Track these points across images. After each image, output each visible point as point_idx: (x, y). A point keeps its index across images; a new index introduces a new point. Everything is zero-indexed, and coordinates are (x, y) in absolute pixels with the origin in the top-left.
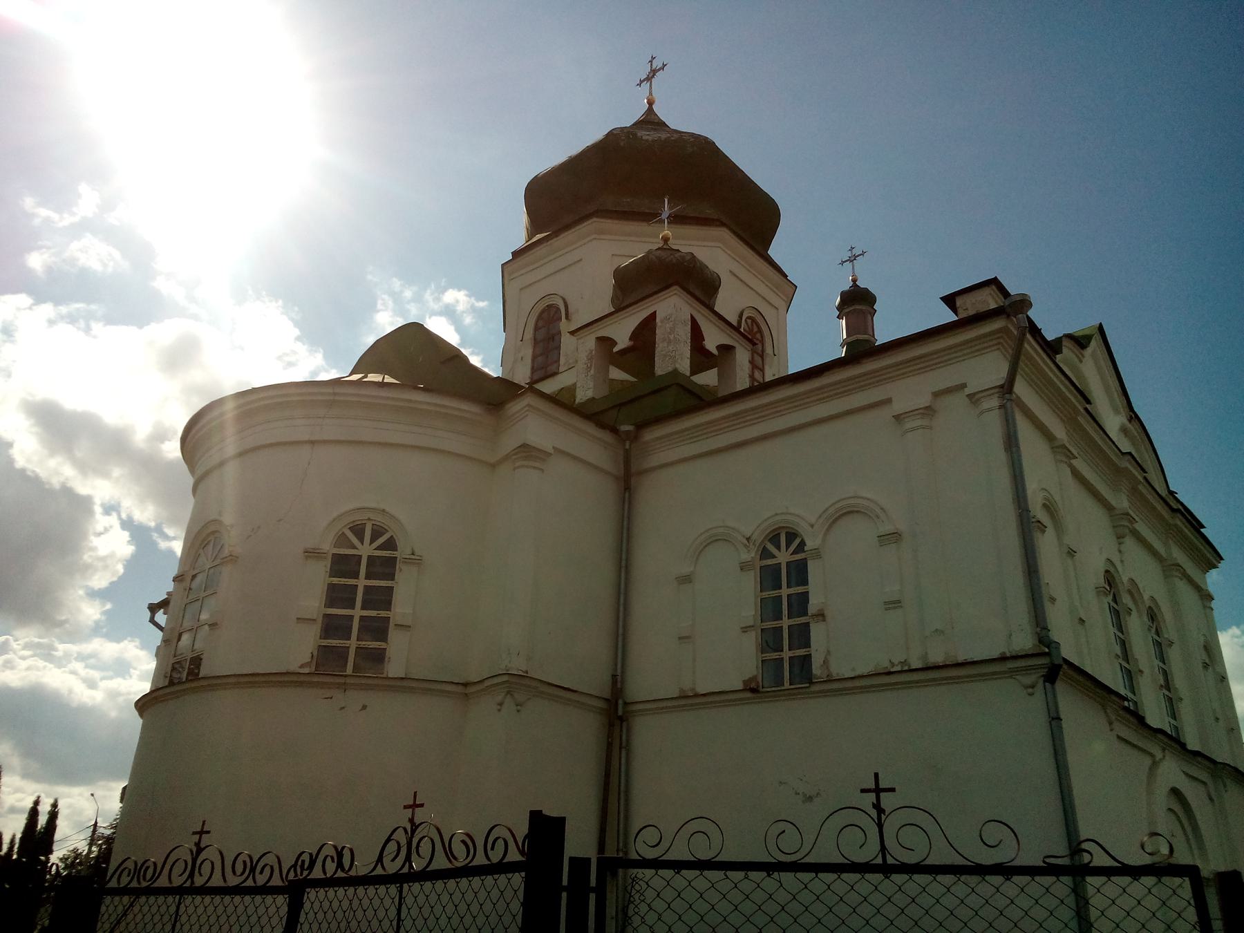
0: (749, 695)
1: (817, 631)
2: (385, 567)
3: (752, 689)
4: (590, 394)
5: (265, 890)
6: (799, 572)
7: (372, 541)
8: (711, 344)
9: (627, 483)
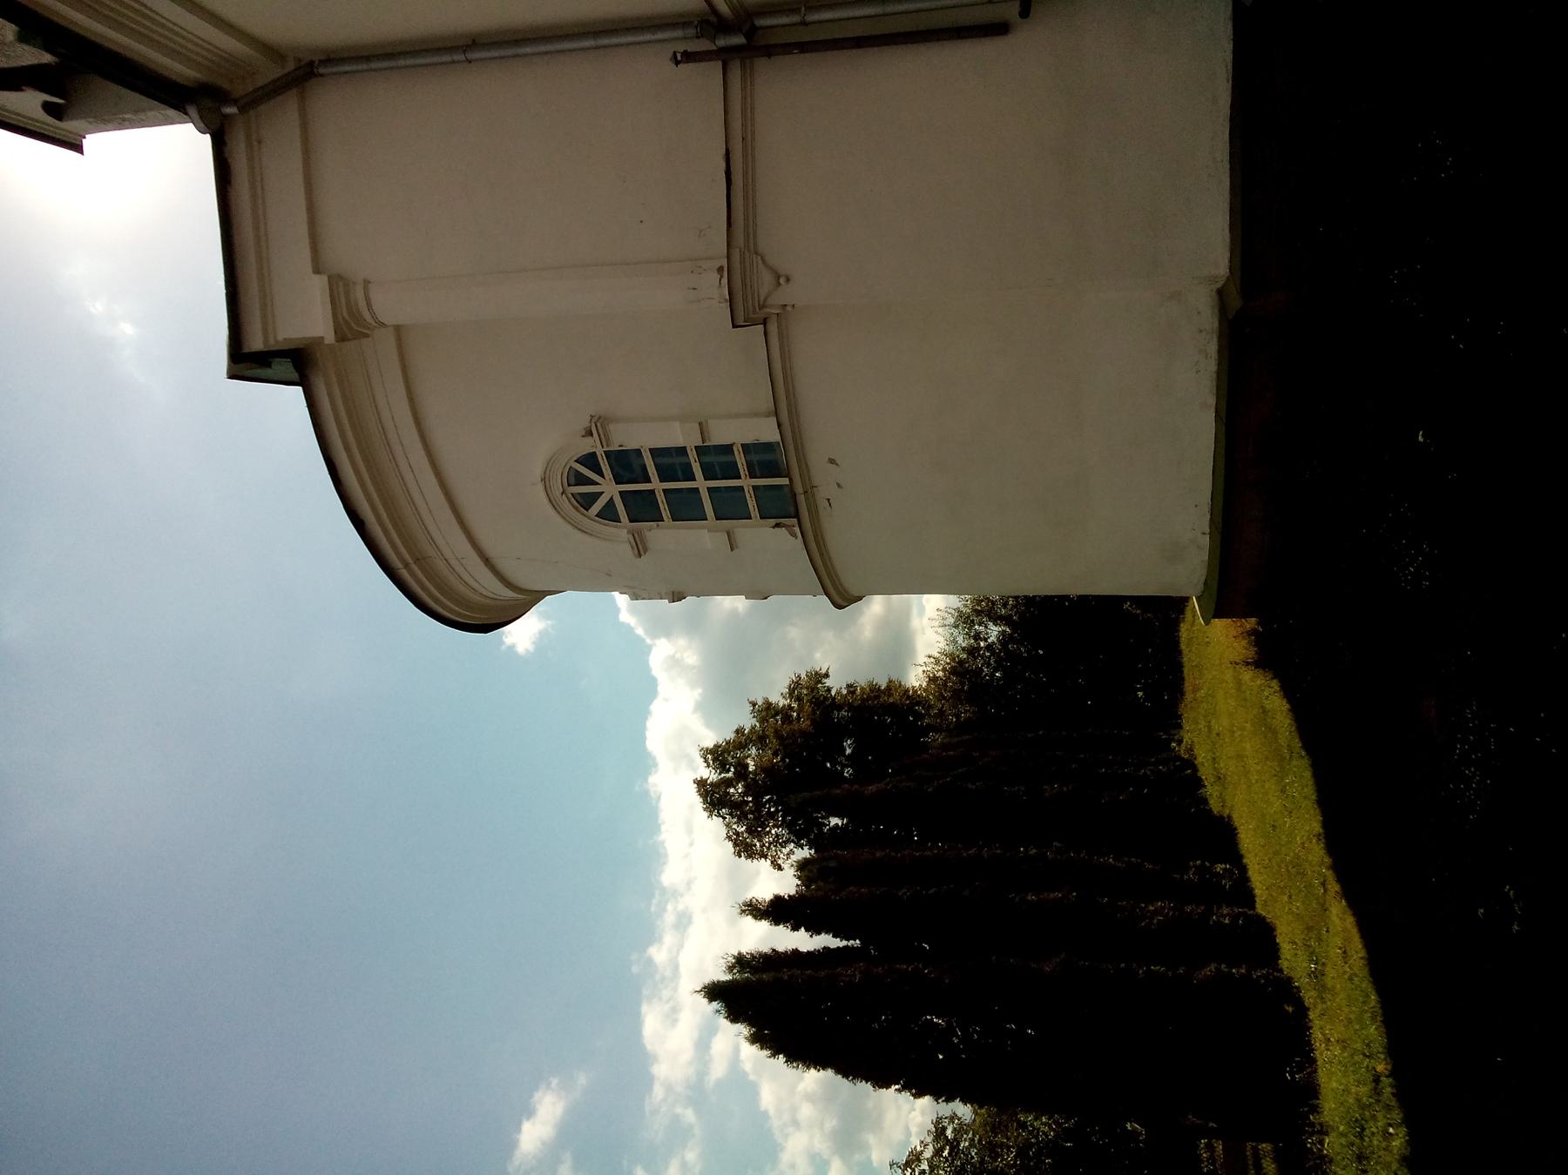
2: (625, 464)
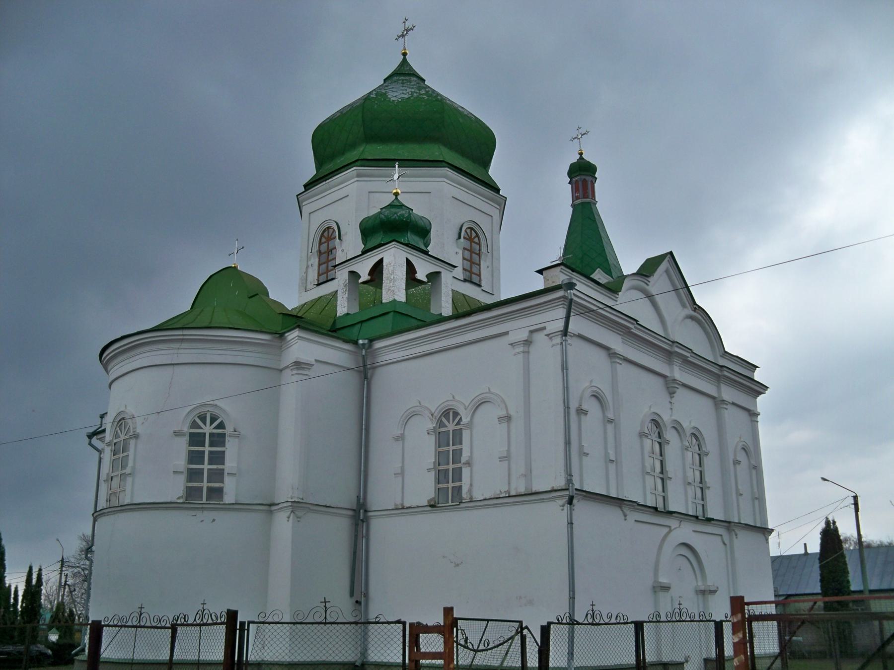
0: (430, 508)
1: (466, 472)
2: (218, 439)
3: (433, 506)
4: (345, 311)
5: (165, 628)
6: (458, 436)
7: (211, 423)
8: (421, 275)
9: (365, 373)
